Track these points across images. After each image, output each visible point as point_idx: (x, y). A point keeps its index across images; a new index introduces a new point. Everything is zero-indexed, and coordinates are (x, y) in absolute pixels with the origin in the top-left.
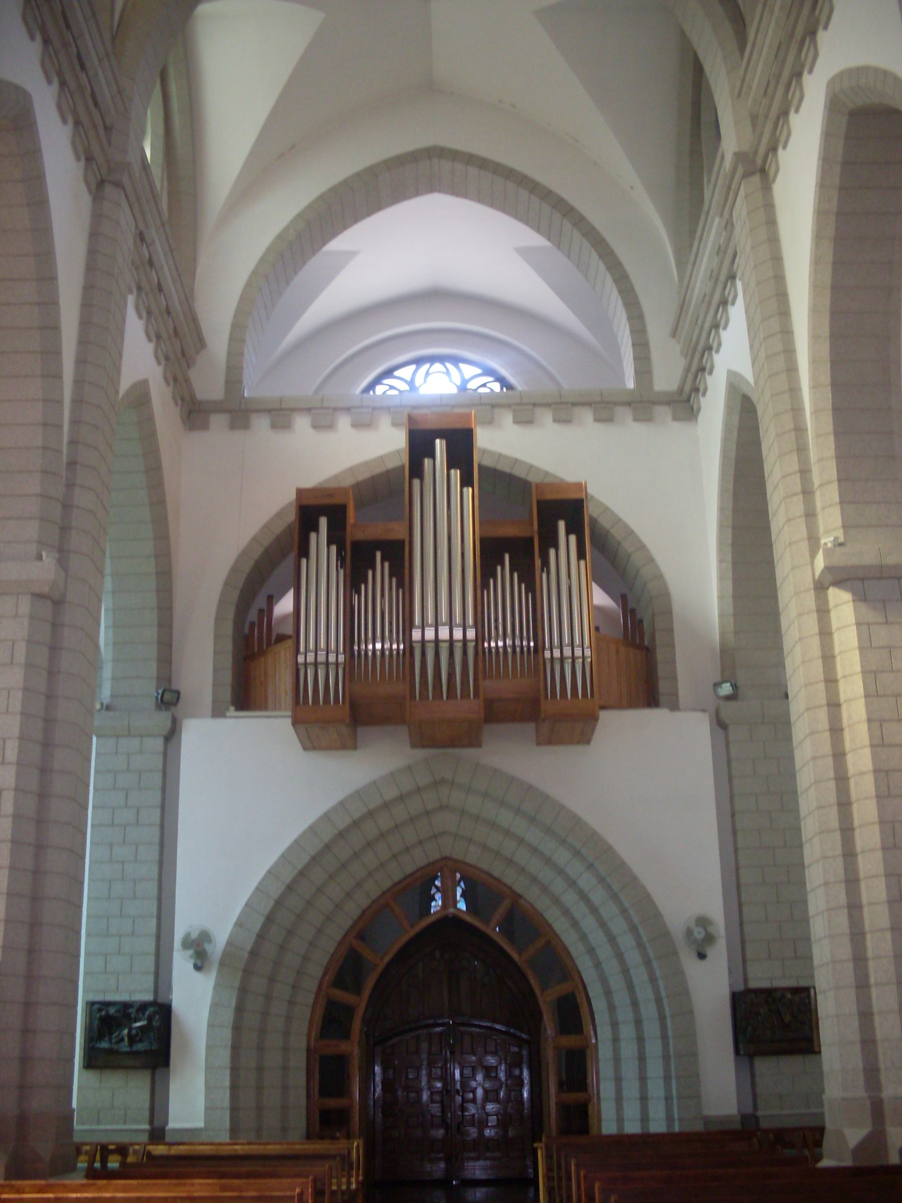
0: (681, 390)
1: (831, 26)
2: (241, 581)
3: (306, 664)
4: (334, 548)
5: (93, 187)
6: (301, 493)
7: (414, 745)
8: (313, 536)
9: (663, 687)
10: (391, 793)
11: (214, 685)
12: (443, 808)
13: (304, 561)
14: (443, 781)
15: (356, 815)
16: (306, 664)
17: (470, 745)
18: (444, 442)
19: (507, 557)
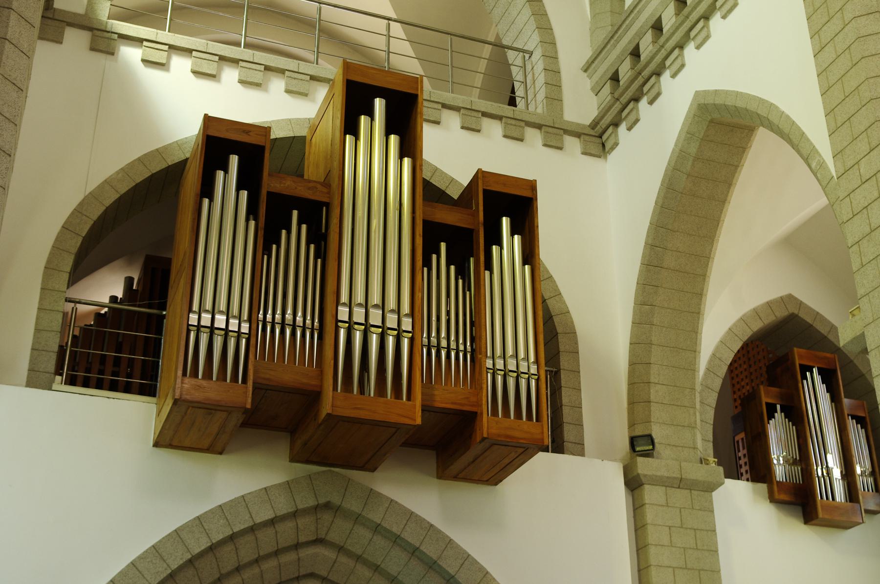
0: (594, 124)
1: (731, 17)
2: (96, 213)
3: (199, 327)
4: (244, 194)
5: (592, 17)
6: (697, 93)
7: (293, 459)
8: (220, 174)
9: (569, 433)
10: (264, 514)
11: (33, 349)
12: (319, 541)
13: (206, 201)
14: (327, 506)
15: (217, 537)
16: (199, 327)
17: (362, 468)
18: (384, 101)
19: (443, 246)
